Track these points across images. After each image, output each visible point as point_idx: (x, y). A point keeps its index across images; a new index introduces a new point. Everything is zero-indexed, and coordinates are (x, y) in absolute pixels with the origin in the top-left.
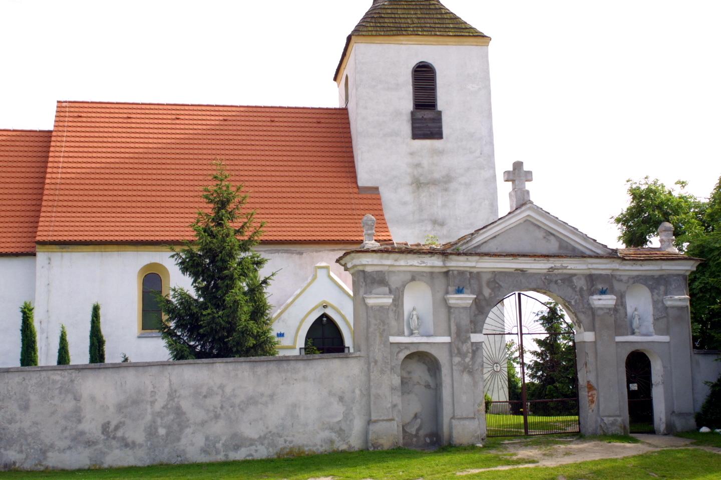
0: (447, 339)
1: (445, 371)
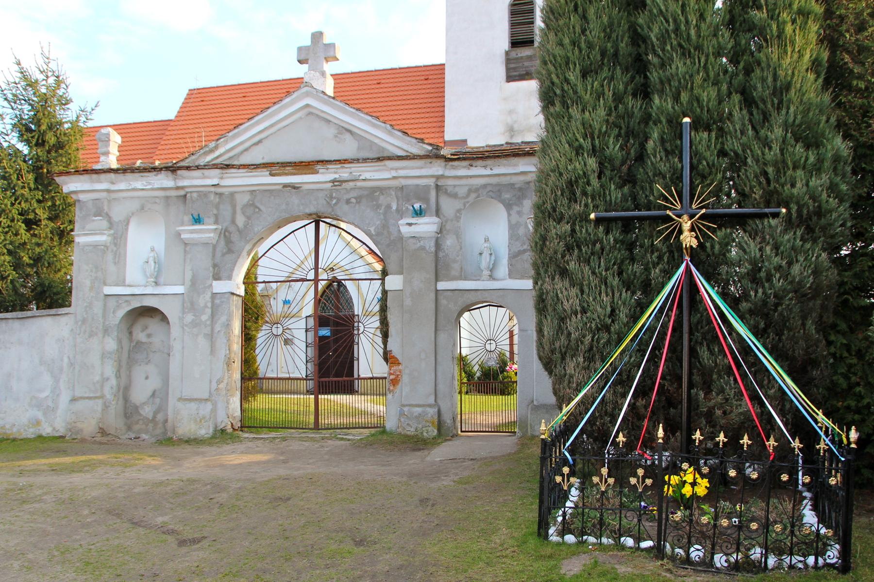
0: (180, 289)
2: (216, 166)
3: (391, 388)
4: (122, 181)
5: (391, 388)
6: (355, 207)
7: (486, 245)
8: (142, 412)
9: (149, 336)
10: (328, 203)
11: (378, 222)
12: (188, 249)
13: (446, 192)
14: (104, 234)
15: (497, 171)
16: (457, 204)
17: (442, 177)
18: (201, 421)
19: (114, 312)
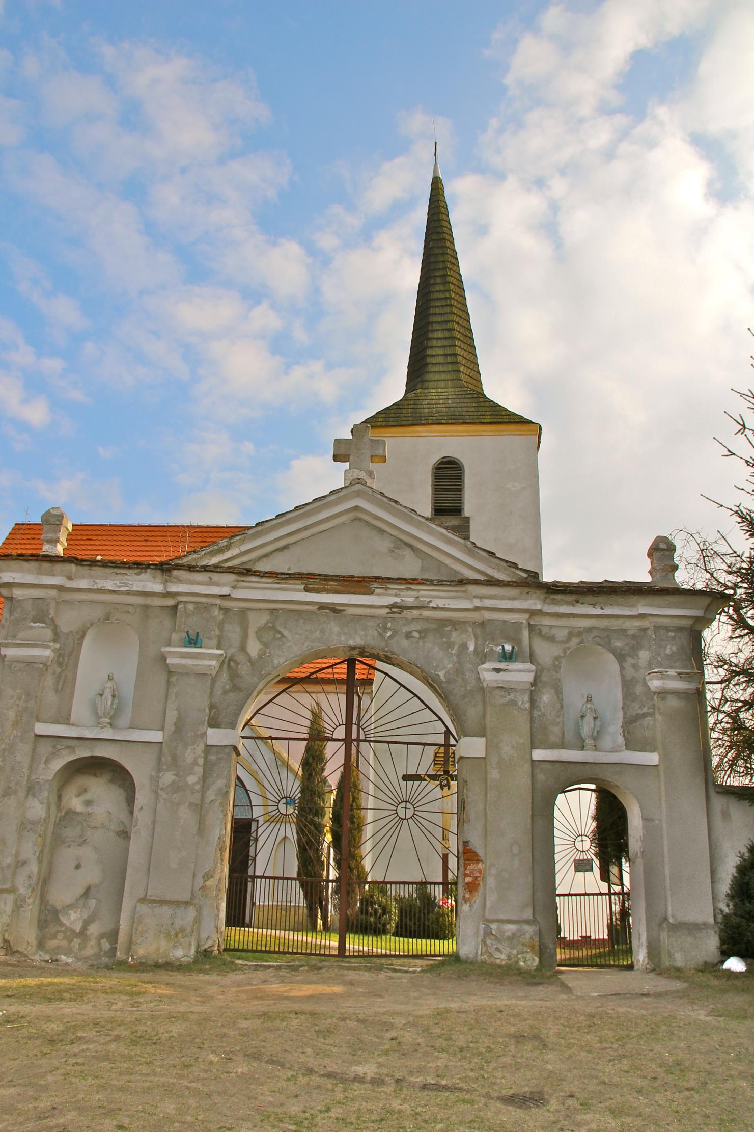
0: (156, 736)
1: (142, 797)
2: (231, 570)
3: (467, 896)
4: (83, 577)
5: (467, 896)
6: (417, 642)
7: (589, 706)
8: (64, 920)
9: (88, 803)
10: (380, 635)
11: (450, 666)
12: (174, 679)
13: (540, 634)
14: (47, 647)
15: (608, 611)
16: (556, 650)
17: (539, 613)
18: (176, 935)
19: (46, 762)
